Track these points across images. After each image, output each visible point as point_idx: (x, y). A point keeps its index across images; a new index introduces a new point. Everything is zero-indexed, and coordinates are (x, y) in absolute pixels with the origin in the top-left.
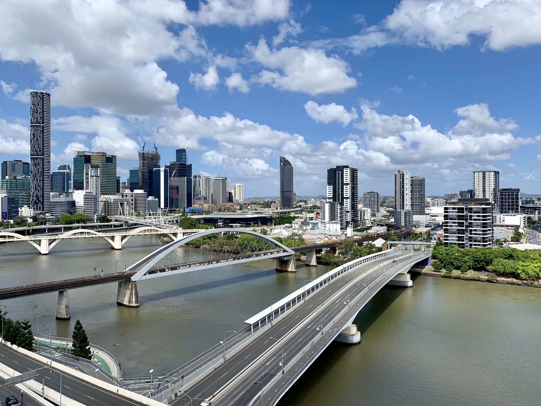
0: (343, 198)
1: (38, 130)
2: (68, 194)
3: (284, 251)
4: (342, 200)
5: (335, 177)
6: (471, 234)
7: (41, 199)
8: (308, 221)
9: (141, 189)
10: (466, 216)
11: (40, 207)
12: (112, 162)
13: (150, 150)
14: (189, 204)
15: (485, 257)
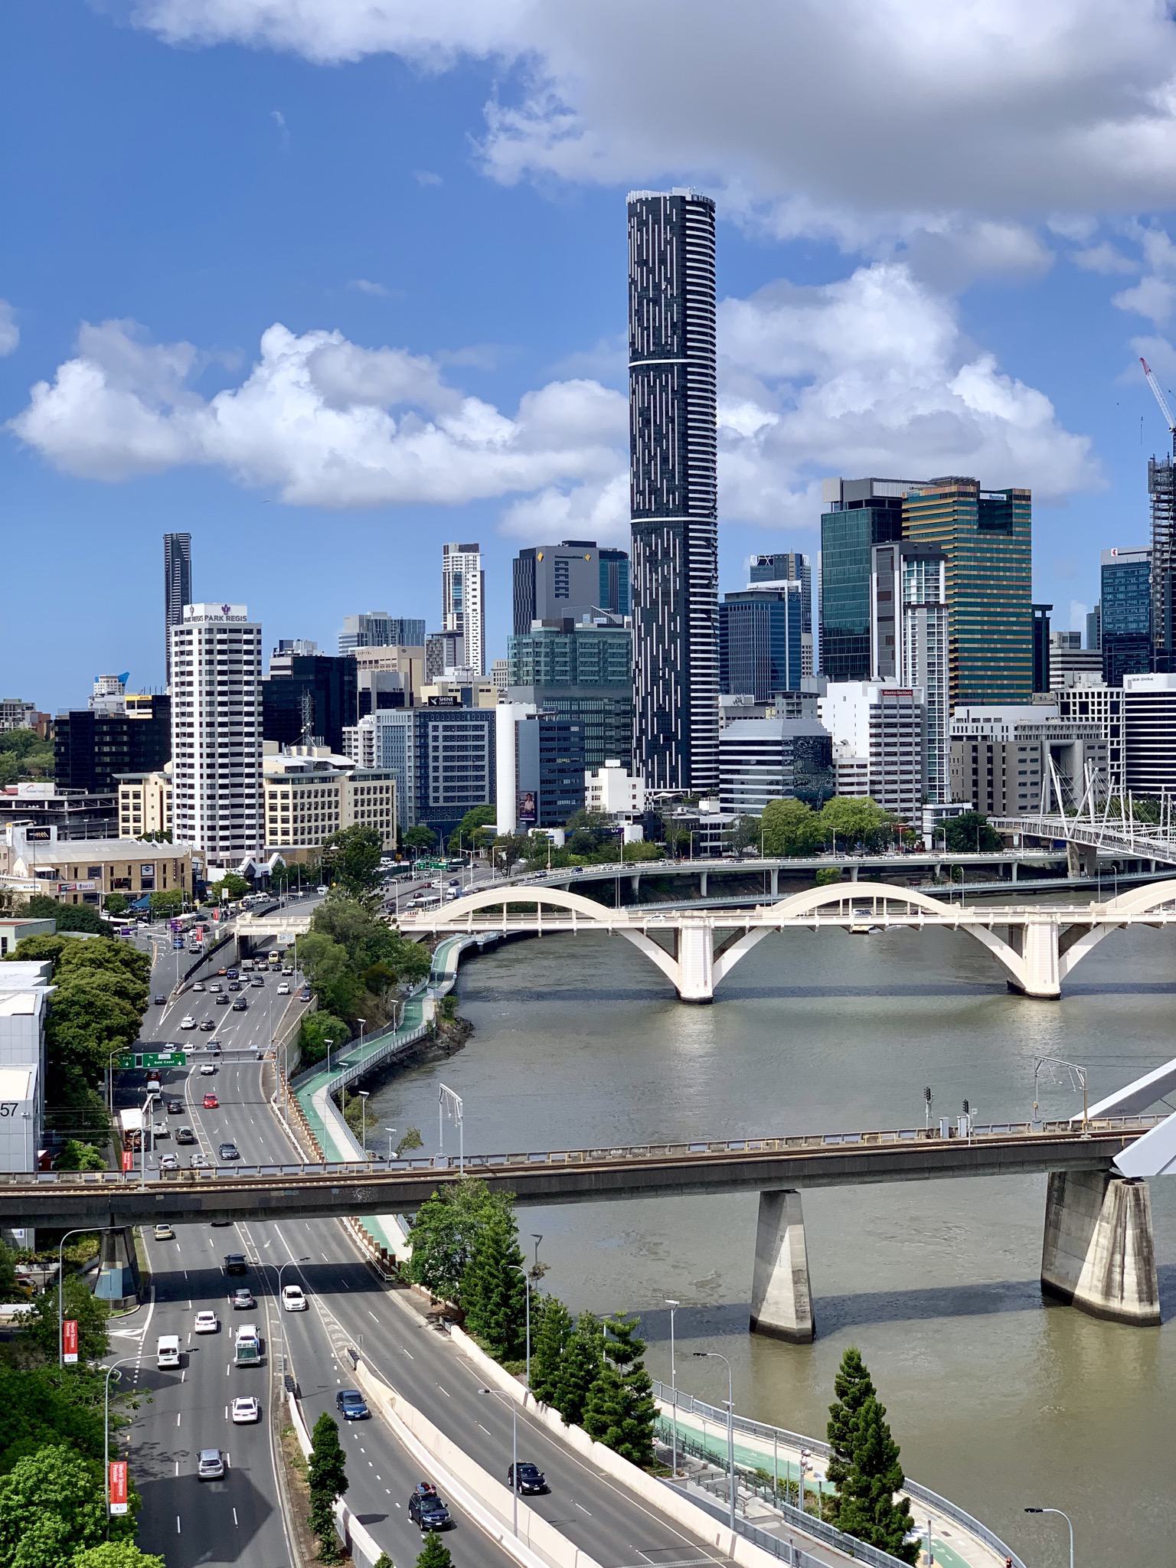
1: (664, 388)
2: (800, 702)
7: (676, 725)
11: (674, 769)
12: (1006, 527)
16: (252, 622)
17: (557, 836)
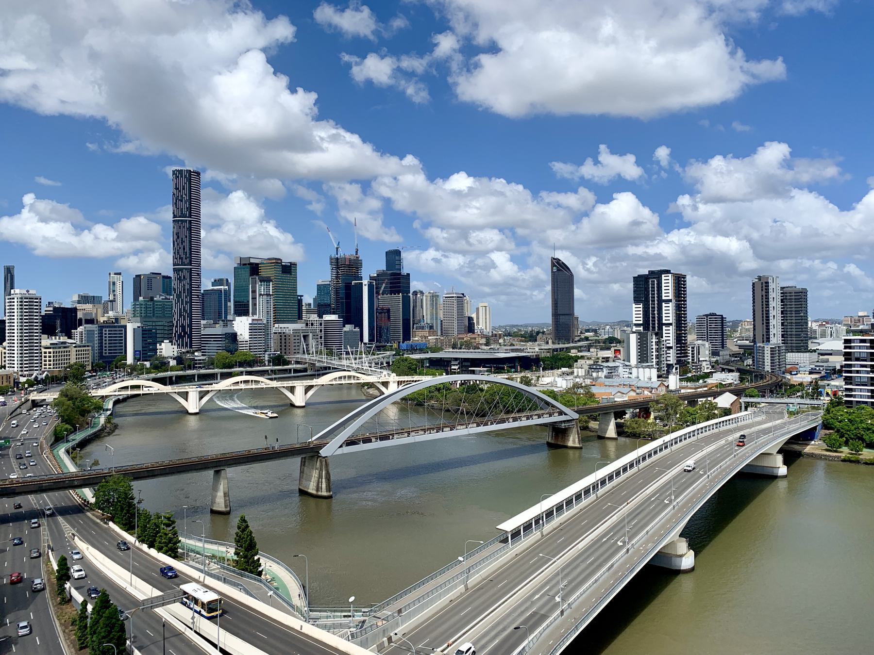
0: (661, 325)
2: (227, 323)
3: (561, 413)
4: (660, 328)
7: (187, 330)
8: (600, 363)
9: (334, 313)
13: (347, 252)
14: (407, 336)
16: (38, 295)
17: (148, 364)
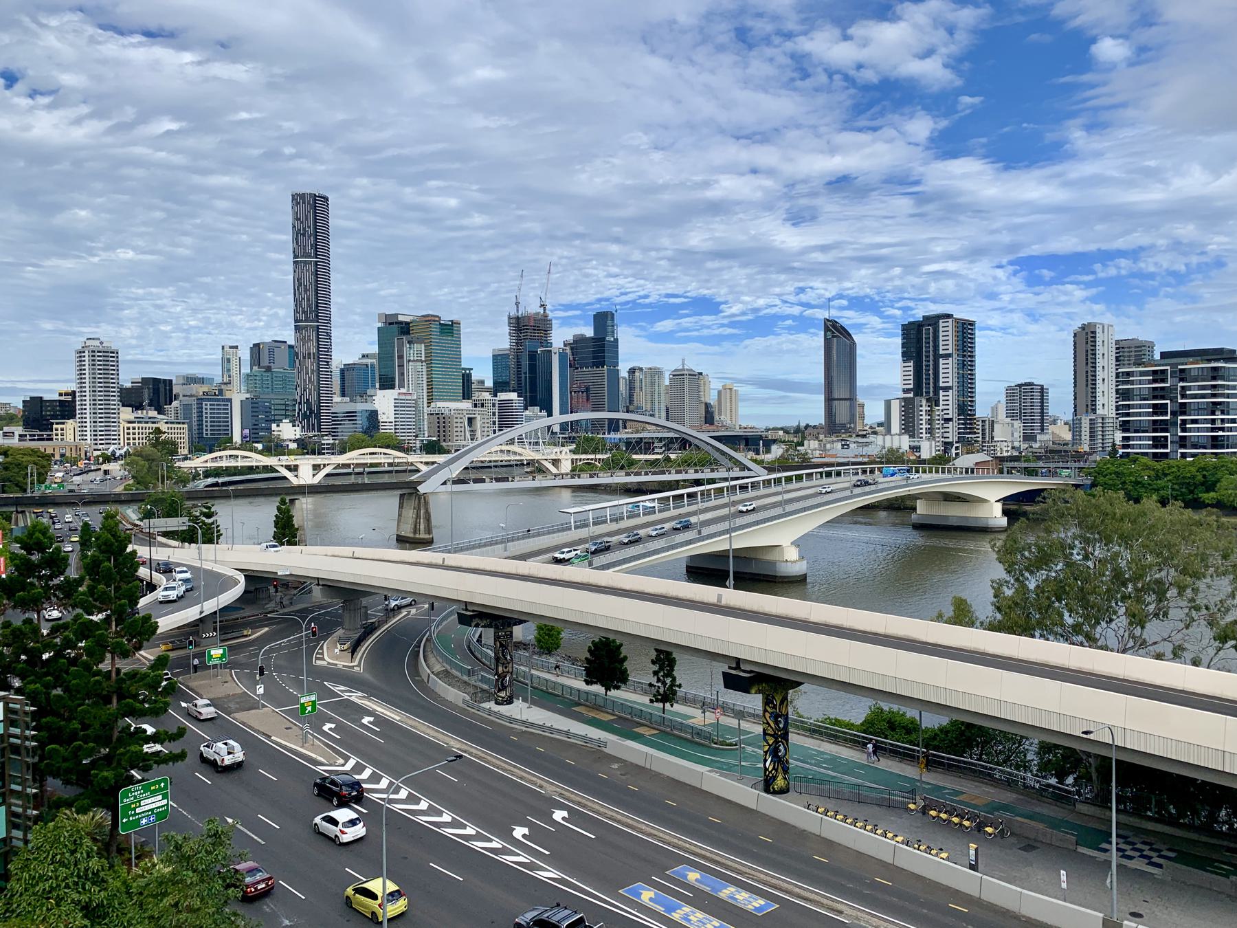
0: (937, 388)
4: (936, 393)
5: (919, 340)
6: (1184, 430)
7: (315, 408)
10: (1172, 389)
12: (451, 333)
15: (1204, 476)
